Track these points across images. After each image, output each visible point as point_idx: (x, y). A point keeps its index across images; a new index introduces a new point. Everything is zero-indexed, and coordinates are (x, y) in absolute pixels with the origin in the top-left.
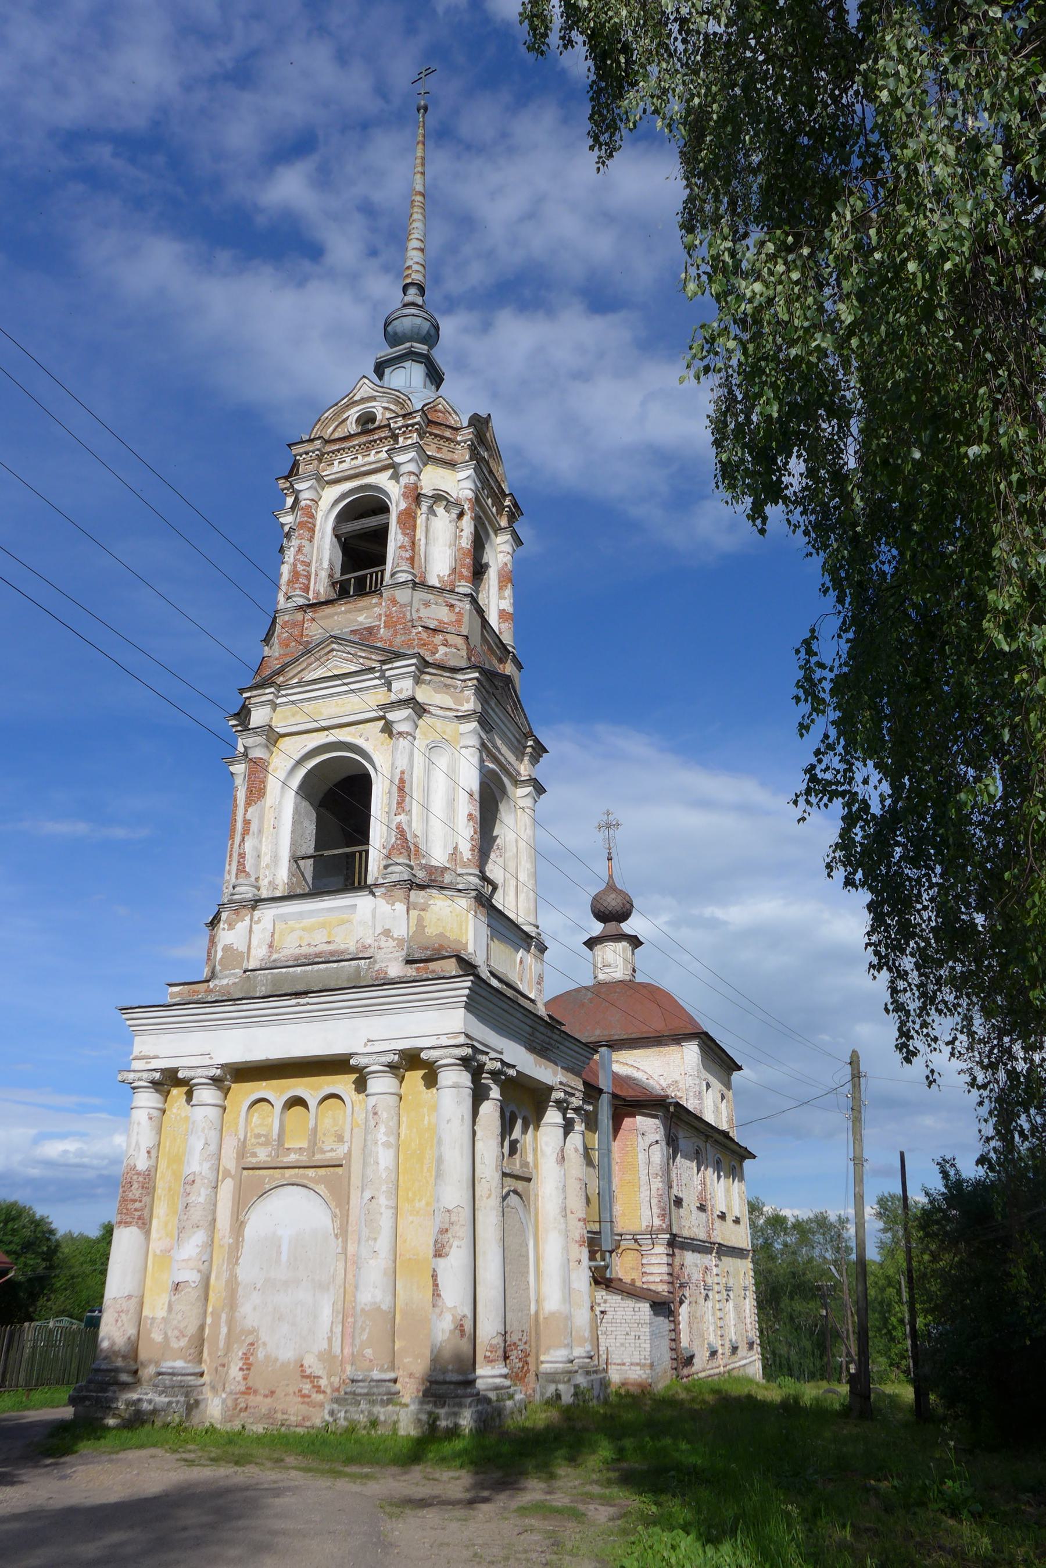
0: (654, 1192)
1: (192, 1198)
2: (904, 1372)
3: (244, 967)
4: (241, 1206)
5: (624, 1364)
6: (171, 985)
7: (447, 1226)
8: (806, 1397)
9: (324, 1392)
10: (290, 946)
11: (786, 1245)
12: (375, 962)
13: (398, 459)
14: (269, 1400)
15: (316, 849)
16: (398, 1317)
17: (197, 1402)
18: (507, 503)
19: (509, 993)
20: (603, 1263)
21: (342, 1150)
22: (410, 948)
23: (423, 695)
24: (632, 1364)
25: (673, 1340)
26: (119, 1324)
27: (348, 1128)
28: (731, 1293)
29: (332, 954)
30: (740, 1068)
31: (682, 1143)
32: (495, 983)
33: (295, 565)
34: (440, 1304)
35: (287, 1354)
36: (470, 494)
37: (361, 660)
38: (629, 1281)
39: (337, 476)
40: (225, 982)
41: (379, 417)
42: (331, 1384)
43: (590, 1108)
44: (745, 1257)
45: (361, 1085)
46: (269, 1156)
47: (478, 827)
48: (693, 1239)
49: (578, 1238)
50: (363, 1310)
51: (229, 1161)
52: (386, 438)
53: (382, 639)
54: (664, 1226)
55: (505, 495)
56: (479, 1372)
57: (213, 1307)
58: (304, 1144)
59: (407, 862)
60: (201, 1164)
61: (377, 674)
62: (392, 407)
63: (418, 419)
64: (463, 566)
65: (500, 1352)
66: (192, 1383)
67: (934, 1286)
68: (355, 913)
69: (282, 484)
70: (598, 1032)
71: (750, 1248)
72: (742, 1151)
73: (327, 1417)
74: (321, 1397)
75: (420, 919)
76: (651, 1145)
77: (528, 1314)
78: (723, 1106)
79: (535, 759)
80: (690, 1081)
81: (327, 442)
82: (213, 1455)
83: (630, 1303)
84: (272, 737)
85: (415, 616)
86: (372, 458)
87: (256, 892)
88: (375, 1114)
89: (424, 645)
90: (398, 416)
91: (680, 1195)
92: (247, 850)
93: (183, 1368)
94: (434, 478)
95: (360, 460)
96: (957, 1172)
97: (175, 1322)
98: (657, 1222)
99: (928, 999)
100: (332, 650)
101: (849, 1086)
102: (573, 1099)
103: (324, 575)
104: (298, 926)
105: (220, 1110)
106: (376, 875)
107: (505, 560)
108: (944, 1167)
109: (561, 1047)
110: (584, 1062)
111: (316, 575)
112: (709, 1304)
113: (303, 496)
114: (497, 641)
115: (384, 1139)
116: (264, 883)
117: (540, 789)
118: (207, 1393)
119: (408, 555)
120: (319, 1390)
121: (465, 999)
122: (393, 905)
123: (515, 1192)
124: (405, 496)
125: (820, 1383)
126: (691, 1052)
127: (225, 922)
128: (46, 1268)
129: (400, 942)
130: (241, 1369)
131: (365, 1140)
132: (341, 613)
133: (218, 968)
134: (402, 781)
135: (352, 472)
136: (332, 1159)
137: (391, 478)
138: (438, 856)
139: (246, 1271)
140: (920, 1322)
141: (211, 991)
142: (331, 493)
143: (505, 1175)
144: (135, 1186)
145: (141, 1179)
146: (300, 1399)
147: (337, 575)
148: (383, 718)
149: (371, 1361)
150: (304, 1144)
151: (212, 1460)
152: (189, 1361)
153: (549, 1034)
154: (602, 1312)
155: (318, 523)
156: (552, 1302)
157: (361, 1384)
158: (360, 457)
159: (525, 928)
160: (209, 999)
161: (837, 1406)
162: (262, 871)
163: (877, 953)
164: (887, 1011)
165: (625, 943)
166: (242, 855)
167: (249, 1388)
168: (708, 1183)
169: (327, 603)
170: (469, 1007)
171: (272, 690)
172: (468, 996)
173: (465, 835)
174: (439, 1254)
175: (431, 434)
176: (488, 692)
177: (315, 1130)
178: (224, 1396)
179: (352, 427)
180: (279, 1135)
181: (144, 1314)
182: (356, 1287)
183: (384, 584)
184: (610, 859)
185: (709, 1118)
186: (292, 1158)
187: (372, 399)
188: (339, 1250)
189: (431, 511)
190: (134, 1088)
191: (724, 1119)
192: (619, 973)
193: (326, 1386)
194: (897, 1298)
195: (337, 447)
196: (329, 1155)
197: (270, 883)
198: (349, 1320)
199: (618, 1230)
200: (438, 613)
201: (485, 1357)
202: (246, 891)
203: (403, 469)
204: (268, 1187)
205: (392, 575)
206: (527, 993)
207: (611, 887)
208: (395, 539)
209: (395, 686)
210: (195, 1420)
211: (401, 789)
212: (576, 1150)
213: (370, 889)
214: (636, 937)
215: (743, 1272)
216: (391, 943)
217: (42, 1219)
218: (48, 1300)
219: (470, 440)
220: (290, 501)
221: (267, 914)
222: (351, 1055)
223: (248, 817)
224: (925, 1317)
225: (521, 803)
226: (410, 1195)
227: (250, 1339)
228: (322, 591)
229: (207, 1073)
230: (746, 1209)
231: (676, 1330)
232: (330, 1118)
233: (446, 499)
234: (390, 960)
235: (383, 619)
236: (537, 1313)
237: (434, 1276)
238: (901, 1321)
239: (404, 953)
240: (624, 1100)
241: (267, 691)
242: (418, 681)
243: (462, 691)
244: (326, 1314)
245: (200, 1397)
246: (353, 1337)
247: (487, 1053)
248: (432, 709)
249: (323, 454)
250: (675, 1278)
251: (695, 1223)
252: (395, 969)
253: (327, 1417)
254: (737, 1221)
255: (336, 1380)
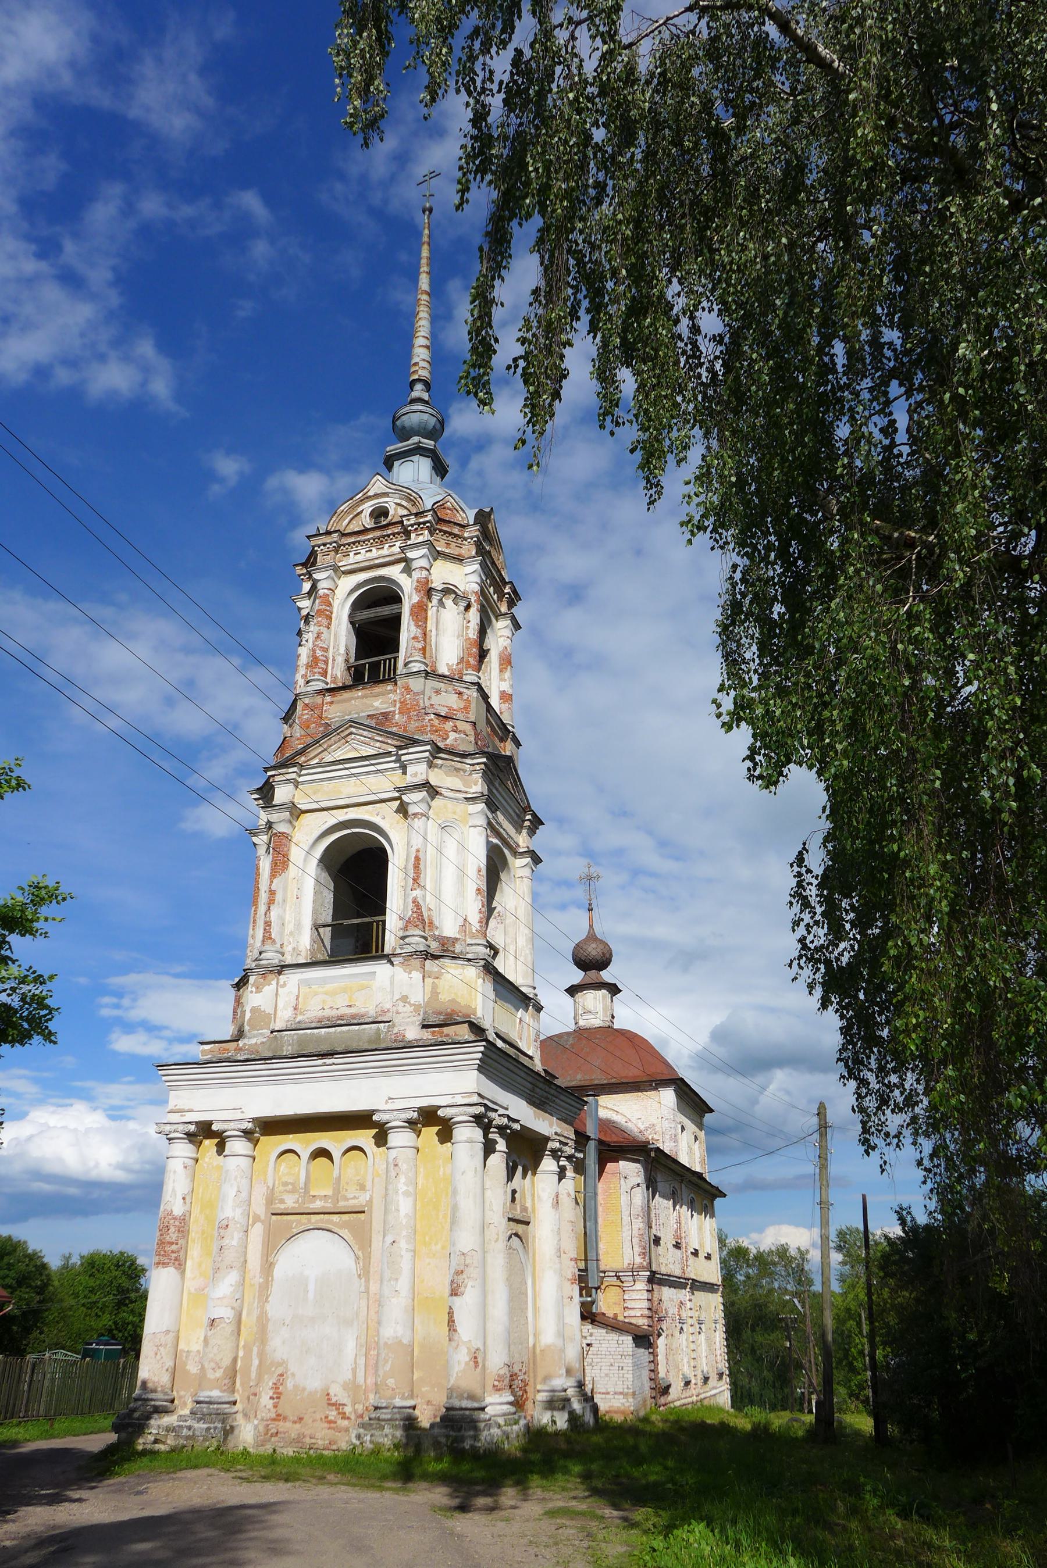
0: (635, 1232)
1: (226, 1242)
2: (862, 1402)
3: (271, 1027)
4: (271, 1247)
5: (608, 1393)
6: (202, 1043)
7: (462, 1268)
8: (774, 1427)
9: (349, 1418)
10: (314, 1009)
11: (748, 1277)
12: (394, 1025)
13: (411, 555)
14: (298, 1426)
15: (334, 917)
16: (416, 1349)
17: (232, 1428)
18: (507, 590)
19: (511, 1051)
20: (589, 1299)
21: (363, 1199)
22: (425, 1013)
23: (436, 778)
24: (615, 1393)
25: (652, 1371)
26: (158, 1357)
27: (369, 1178)
28: (703, 1326)
29: (353, 1017)
30: (711, 1111)
31: (660, 1185)
32: (500, 1044)
33: (314, 651)
34: (456, 1338)
35: (314, 1383)
36: (476, 588)
37: (378, 744)
38: (611, 1316)
39: (353, 567)
40: (253, 1041)
41: (391, 512)
42: (355, 1411)
43: (581, 1155)
44: (715, 1291)
45: (381, 1139)
46: (297, 1202)
47: (485, 900)
48: (669, 1276)
49: (570, 1277)
50: (386, 1344)
51: (259, 1207)
52: (398, 533)
53: (397, 725)
54: (645, 1264)
55: (505, 583)
56: (488, 1400)
57: (245, 1341)
58: (329, 1192)
59: (423, 934)
60: (234, 1210)
61: (393, 758)
62: (404, 503)
63: (429, 518)
64: (469, 655)
65: (507, 1382)
66: (227, 1411)
67: (892, 1319)
68: (374, 979)
69: (300, 570)
70: (579, 1077)
71: (720, 1283)
72: (714, 1191)
73: (354, 1441)
74: (346, 1423)
75: (434, 987)
76: (632, 1188)
77: (528, 1347)
78: (696, 1146)
79: (532, 832)
80: (666, 1124)
81: (344, 535)
82: (263, 1473)
83: (614, 1336)
84: (296, 812)
85: (427, 704)
86: (385, 551)
87: (282, 958)
88: (396, 1165)
89: (436, 731)
90: (411, 514)
91: (658, 1234)
92: (272, 919)
93: (220, 1397)
94: (443, 573)
95: (375, 553)
96: (913, 1219)
97: (211, 1355)
98: (638, 1260)
99: (883, 1101)
100: (351, 733)
101: (816, 1136)
102: (566, 1148)
103: (340, 660)
104: (320, 990)
105: (251, 1160)
106: (393, 944)
107: (505, 644)
108: (902, 1215)
109: (557, 1100)
110: (575, 1114)
111: (334, 660)
112: (684, 1336)
113: (320, 585)
114: (499, 722)
115: (405, 1188)
116: (288, 949)
117: (536, 860)
118: (240, 1420)
119: (420, 645)
120: (344, 1416)
121: (478, 1062)
122: (410, 973)
123: (516, 1235)
124: (417, 589)
125: (783, 1413)
126: (668, 1096)
127: (253, 985)
128: (40, 1302)
129: (417, 1008)
130: (271, 1398)
131: (386, 1189)
132: (358, 697)
133: (247, 1028)
134: (417, 858)
135: (367, 564)
136: (354, 1206)
137: (402, 572)
138: (449, 928)
139: (276, 1308)
140: (879, 1353)
141: (241, 1049)
142: (348, 583)
143: (510, 1219)
144: (172, 1229)
145: (177, 1223)
146: (326, 1425)
147: (352, 660)
148: (399, 798)
149: (393, 1390)
150: (329, 1192)
151: (264, 1477)
152: (225, 1391)
153: (547, 1089)
154: (588, 1345)
155: (335, 610)
156: (548, 1337)
157: (384, 1411)
158: (374, 549)
159: (523, 989)
160: (239, 1058)
161: (801, 1433)
162: (286, 938)
163: (846, 1066)
164: (854, 1110)
165: (604, 991)
166: (268, 924)
167: (279, 1415)
168: (683, 1222)
169: (345, 688)
170: (481, 1069)
171: (295, 769)
172: (480, 1060)
173: (473, 908)
174: (454, 1293)
175: (441, 531)
176: (493, 774)
177: (339, 1179)
178: (256, 1422)
179: (368, 522)
180: (305, 1184)
181: (180, 1347)
182: (379, 1323)
183: (398, 672)
184: (590, 910)
185: (684, 1160)
186: (318, 1205)
187: (385, 494)
188: (362, 1289)
189: (441, 603)
190: (169, 1139)
191: (697, 1160)
192: (596, 1021)
193: (350, 1413)
194: (857, 1331)
195: (352, 540)
196: (352, 1202)
197: (294, 949)
198: (372, 1352)
199: (602, 1268)
200: (448, 700)
201: (494, 1386)
202: (271, 957)
203: (415, 564)
204: (295, 1231)
205: (406, 665)
206: (525, 1050)
207: (592, 937)
208: (408, 630)
209: (410, 769)
210: (231, 1445)
211: (416, 866)
212: (569, 1195)
213: (389, 958)
214: (615, 985)
215: (713, 1305)
216: (409, 1008)
217: (35, 1253)
218: (41, 1333)
219: (477, 536)
220: (307, 586)
221: (292, 978)
222: (373, 1112)
223: (273, 888)
224: (884, 1349)
225: (520, 873)
226: (427, 1239)
227: (280, 1371)
228: (339, 675)
229: (239, 1126)
230: (716, 1245)
231: (654, 1362)
232: (346, 1168)
233: (455, 593)
234: (407, 1024)
235: (398, 705)
236: (534, 1346)
237: (451, 1314)
238: (861, 1353)
239: (420, 1018)
240: (609, 1146)
241: (291, 770)
242: (431, 765)
243: (470, 774)
244: (350, 1347)
245: (235, 1424)
246: (377, 1371)
247: (496, 1111)
248: (443, 791)
249: (339, 547)
250: (655, 1313)
251: (671, 1260)
252: (413, 1033)
253: (354, 1441)
254: (708, 1257)
255: (360, 1408)
